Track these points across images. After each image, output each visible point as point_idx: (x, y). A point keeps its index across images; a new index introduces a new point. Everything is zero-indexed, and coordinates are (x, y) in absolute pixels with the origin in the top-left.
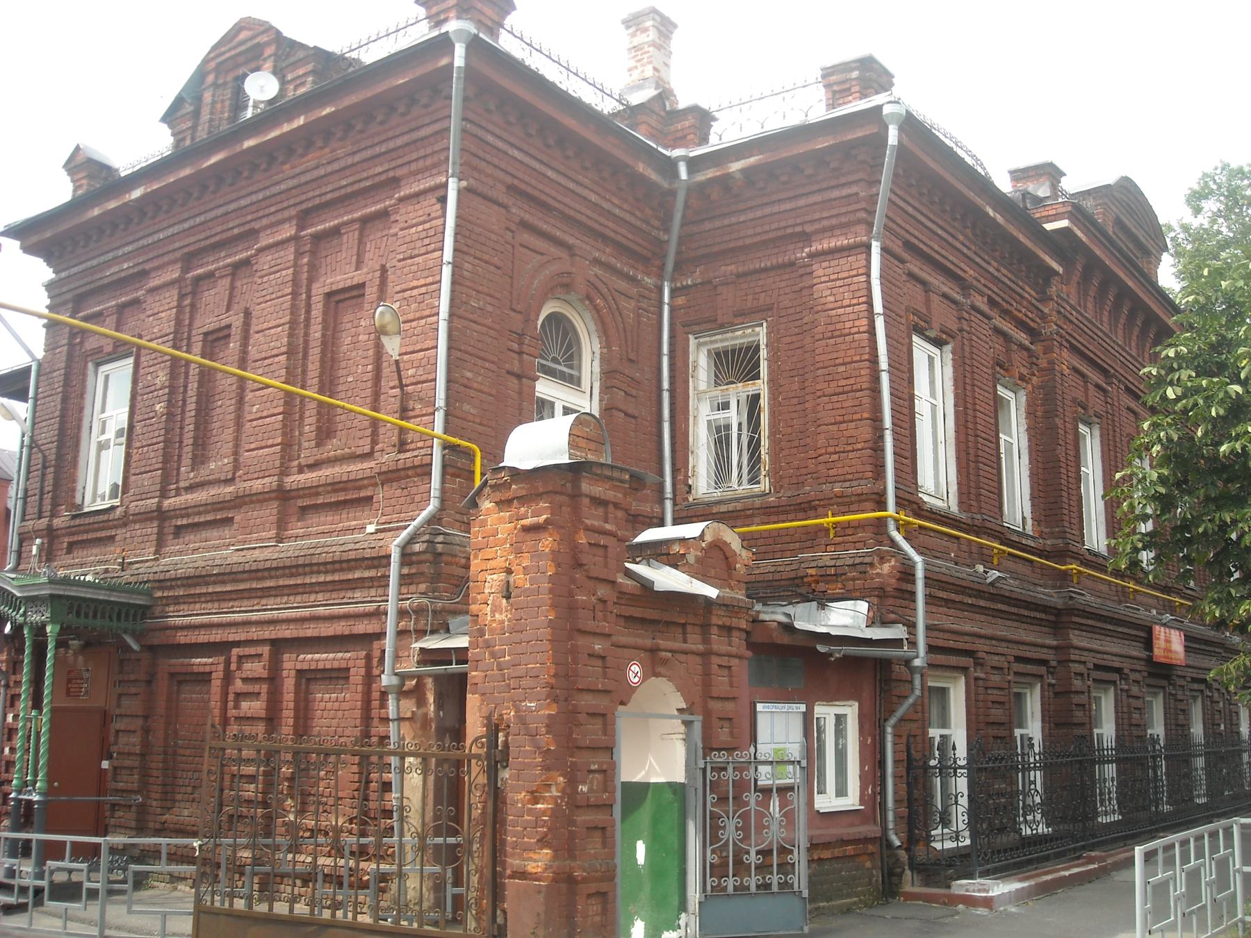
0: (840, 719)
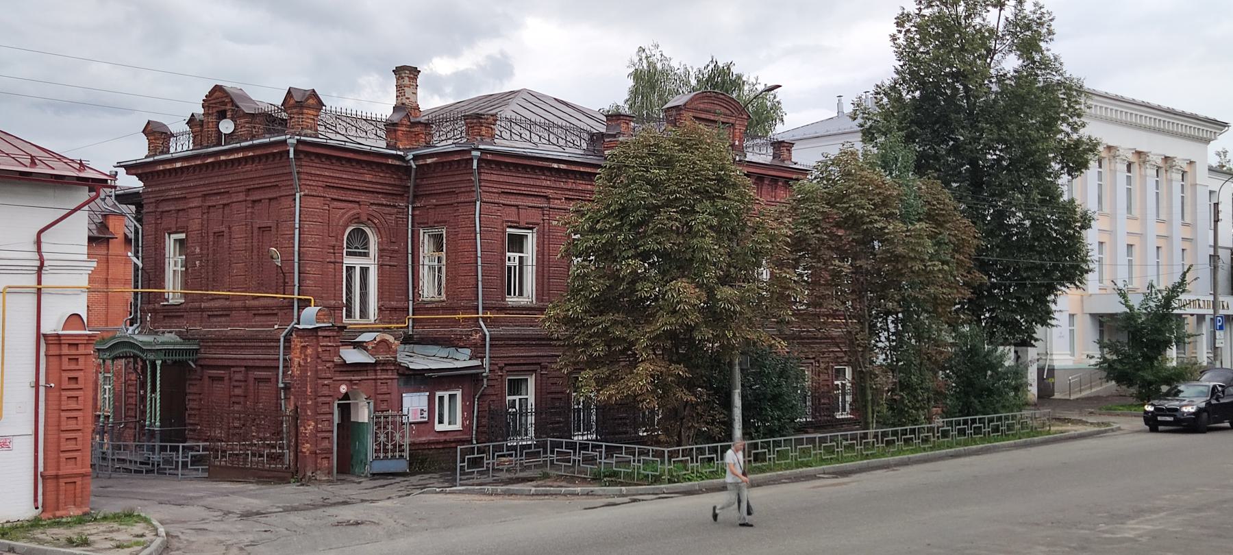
0: (452, 397)
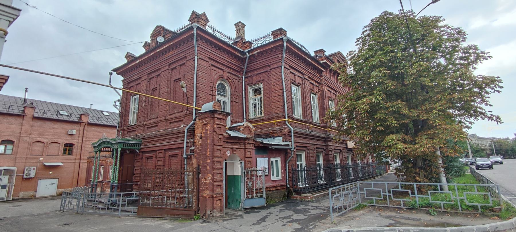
0: (277, 161)
